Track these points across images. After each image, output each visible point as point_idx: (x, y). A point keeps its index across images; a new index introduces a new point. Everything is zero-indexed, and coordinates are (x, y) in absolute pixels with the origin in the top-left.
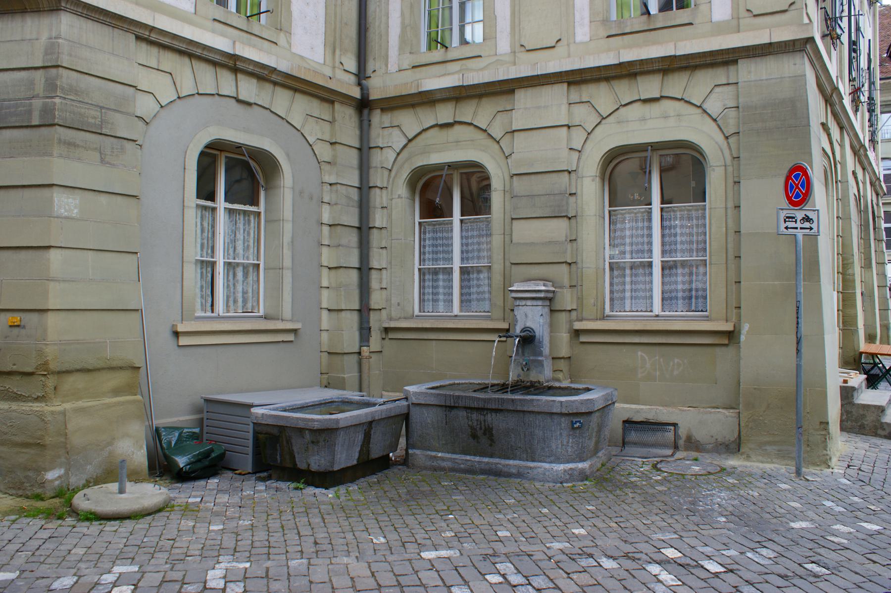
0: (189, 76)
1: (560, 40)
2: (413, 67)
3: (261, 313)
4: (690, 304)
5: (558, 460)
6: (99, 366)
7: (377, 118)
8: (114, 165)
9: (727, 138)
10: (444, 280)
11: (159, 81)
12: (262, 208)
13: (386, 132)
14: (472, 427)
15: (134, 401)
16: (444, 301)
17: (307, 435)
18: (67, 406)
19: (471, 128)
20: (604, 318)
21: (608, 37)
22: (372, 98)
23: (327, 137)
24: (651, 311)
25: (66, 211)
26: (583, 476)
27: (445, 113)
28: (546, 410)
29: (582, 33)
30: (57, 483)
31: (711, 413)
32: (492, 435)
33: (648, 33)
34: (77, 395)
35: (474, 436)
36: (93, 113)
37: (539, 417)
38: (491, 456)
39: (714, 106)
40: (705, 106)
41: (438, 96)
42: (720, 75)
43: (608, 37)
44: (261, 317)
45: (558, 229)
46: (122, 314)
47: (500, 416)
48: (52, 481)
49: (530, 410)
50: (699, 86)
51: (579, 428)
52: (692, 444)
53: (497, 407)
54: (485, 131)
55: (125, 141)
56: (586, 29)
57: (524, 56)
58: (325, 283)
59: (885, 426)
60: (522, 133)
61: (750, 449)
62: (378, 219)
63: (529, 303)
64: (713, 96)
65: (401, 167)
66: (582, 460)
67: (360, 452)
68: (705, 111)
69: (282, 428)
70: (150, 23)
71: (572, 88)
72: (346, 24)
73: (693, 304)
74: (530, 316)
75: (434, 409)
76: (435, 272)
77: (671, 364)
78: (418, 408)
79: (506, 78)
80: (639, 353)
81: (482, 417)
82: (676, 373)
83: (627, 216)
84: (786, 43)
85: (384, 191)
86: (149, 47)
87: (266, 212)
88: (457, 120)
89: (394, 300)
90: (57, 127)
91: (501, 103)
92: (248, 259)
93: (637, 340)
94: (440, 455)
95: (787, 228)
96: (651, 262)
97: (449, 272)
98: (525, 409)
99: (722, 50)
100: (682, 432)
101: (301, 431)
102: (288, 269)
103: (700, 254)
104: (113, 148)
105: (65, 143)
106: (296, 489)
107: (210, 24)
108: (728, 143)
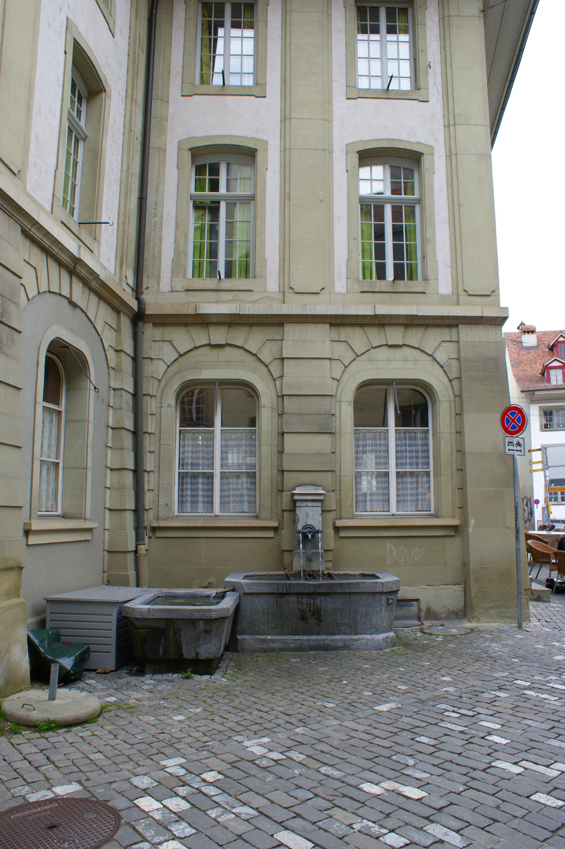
1: (323, 288)
2: (187, 290)
3: (59, 512)
4: (417, 505)
5: (378, 632)
7: (149, 332)
9: (450, 381)
10: (203, 483)
12: (257, 428)
13: (156, 345)
14: (301, 610)
16: (204, 502)
17: (201, 625)
19: (242, 351)
21: (362, 292)
22: (147, 312)
24: (388, 511)
27: (218, 335)
28: (370, 590)
29: (340, 286)
31: (444, 589)
32: (320, 615)
33: (393, 294)
35: (303, 618)
37: (363, 597)
38: (318, 634)
39: (441, 356)
40: (435, 356)
41: (214, 320)
42: (446, 334)
43: (362, 292)
44: (59, 516)
45: (322, 443)
47: (328, 599)
49: (356, 591)
50: (432, 339)
51: (391, 603)
52: (431, 615)
53: (326, 591)
54: (255, 355)
56: (344, 283)
57: (290, 296)
59: (534, 592)
60: (291, 361)
61: (480, 613)
62: (150, 425)
63: (310, 504)
64: (441, 348)
65: (172, 378)
68: (435, 359)
69: (170, 622)
71: (333, 328)
72: (130, 242)
73: (420, 505)
74: (310, 515)
75: (266, 597)
76: (195, 476)
77: (413, 552)
78: (249, 597)
79: (279, 313)
80: (388, 545)
81: (312, 601)
82: (416, 559)
83: (368, 434)
84: (491, 318)
85: (153, 399)
87: (66, 411)
88: (228, 342)
89: (162, 501)
91: (272, 333)
93: (386, 534)
94: (269, 637)
95: (509, 450)
96: (388, 472)
97: (210, 477)
98: (352, 591)
99: (450, 316)
100: (423, 606)
101: (193, 622)
103: (424, 467)
107: (60, 223)
108: (452, 385)
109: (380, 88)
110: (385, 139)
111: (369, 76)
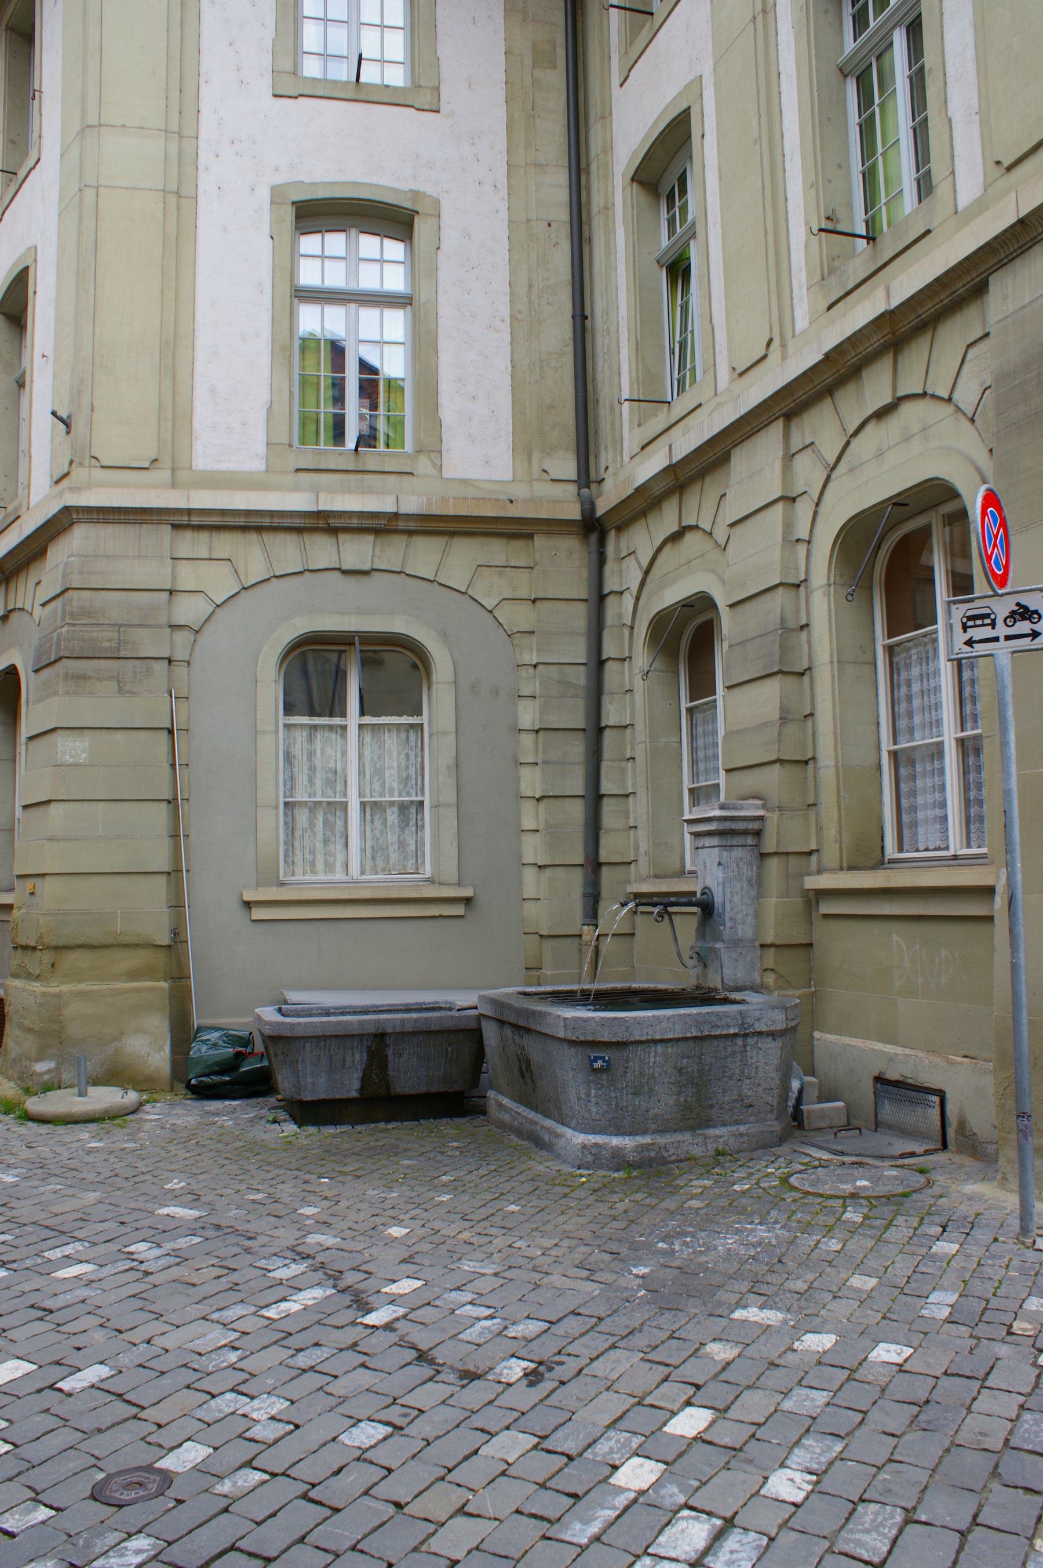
0: (254, 556)
1: (156, 460)
2: (643, 448)
6: (106, 942)
8: (135, 693)
11: (208, 573)
12: (425, 719)
15: (154, 989)
18: (65, 988)
20: (880, 863)
21: (829, 308)
23: (524, 593)
25: (71, 757)
26: (618, 1161)
30: (46, 1077)
34: (79, 976)
36: (108, 635)
43: (829, 308)
44: (427, 880)
46: (143, 877)
48: (41, 1074)
55: (153, 661)
58: (528, 823)
66: (620, 1132)
67: (363, 1080)
70: (182, 505)
80: (895, 937)
86: (196, 534)
90: (64, 660)
92: (408, 794)
102: (448, 806)
104: (135, 673)
105: (73, 677)
106: (275, 1121)
107: (290, 478)
109: (345, 78)
110: (348, 183)
111: (382, 61)
